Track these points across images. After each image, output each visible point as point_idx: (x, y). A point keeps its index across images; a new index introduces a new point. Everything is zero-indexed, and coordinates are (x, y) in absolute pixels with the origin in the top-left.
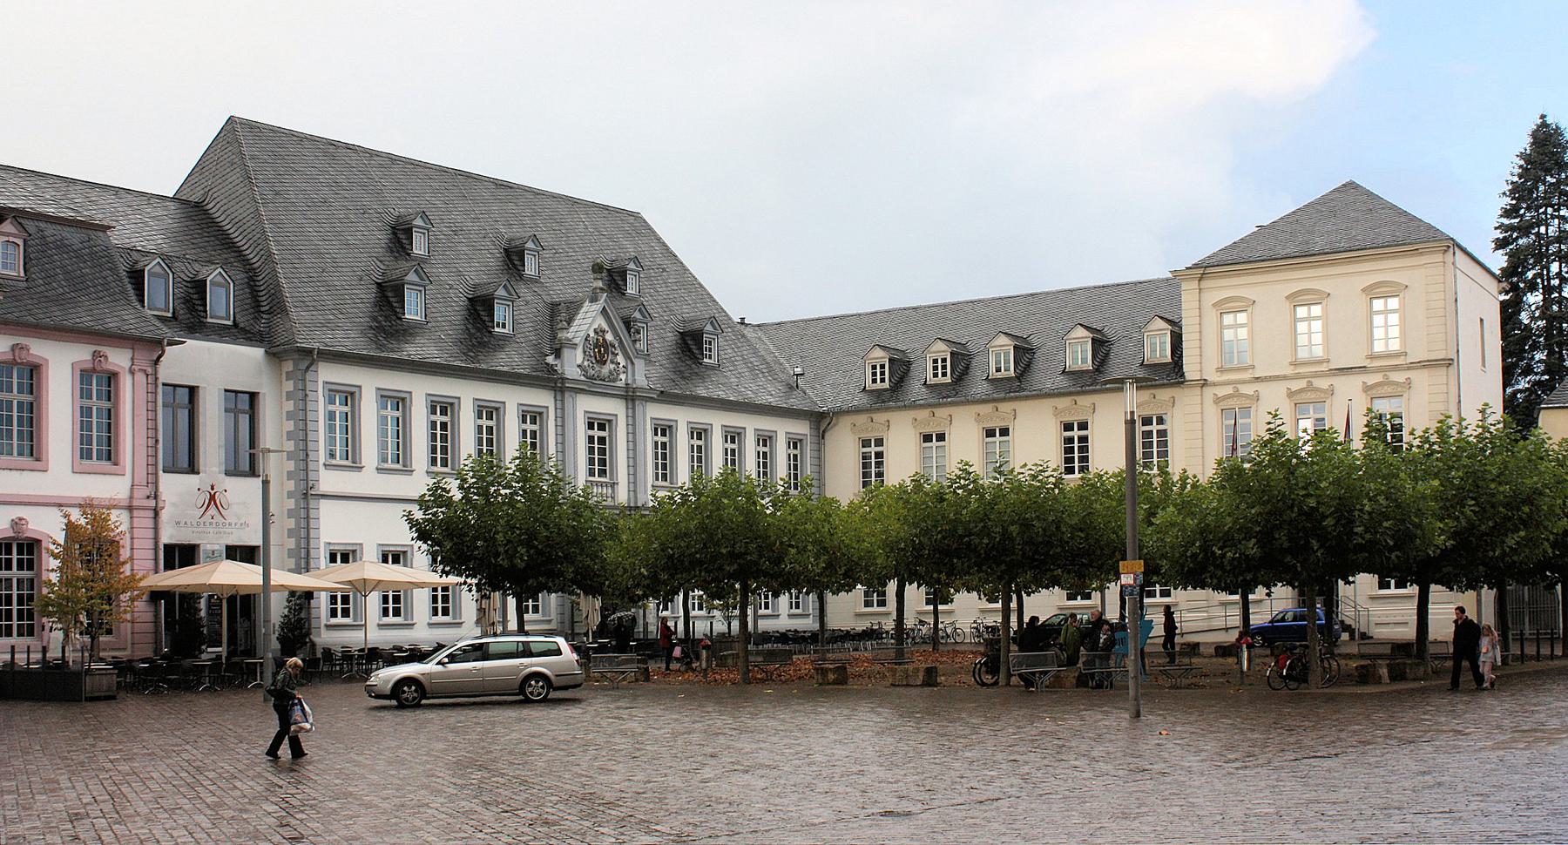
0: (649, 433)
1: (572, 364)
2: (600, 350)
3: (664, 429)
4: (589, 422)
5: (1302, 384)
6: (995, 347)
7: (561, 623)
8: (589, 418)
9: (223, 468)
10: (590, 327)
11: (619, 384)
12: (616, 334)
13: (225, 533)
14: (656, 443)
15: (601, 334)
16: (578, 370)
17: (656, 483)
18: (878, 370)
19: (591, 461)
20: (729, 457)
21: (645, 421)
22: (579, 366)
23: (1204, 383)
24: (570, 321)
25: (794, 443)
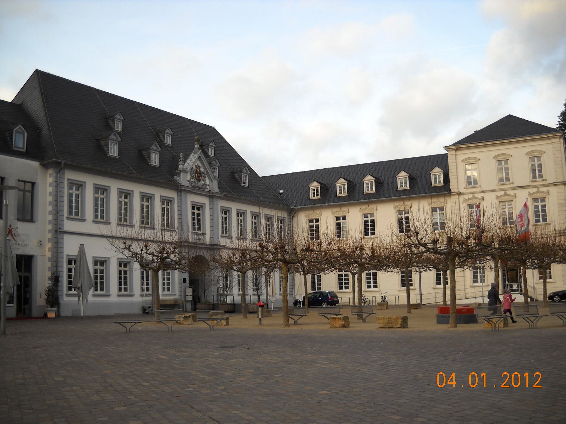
0: (220, 212)
1: (184, 179)
2: (197, 175)
3: (226, 211)
4: (193, 206)
5: (502, 193)
6: (366, 180)
7: (180, 296)
8: (193, 204)
9: (16, 217)
10: (193, 164)
11: (206, 190)
12: (205, 168)
13: (16, 248)
14: (223, 217)
15: (198, 168)
16: (188, 183)
17: (223, 235)
18: (316, 191)
19: (194, 224)
20: (254, 225)
21: (218, 208)
22: (188, 181)
23: (460, 194)
24: (184, 161)
25: (281, 221)
